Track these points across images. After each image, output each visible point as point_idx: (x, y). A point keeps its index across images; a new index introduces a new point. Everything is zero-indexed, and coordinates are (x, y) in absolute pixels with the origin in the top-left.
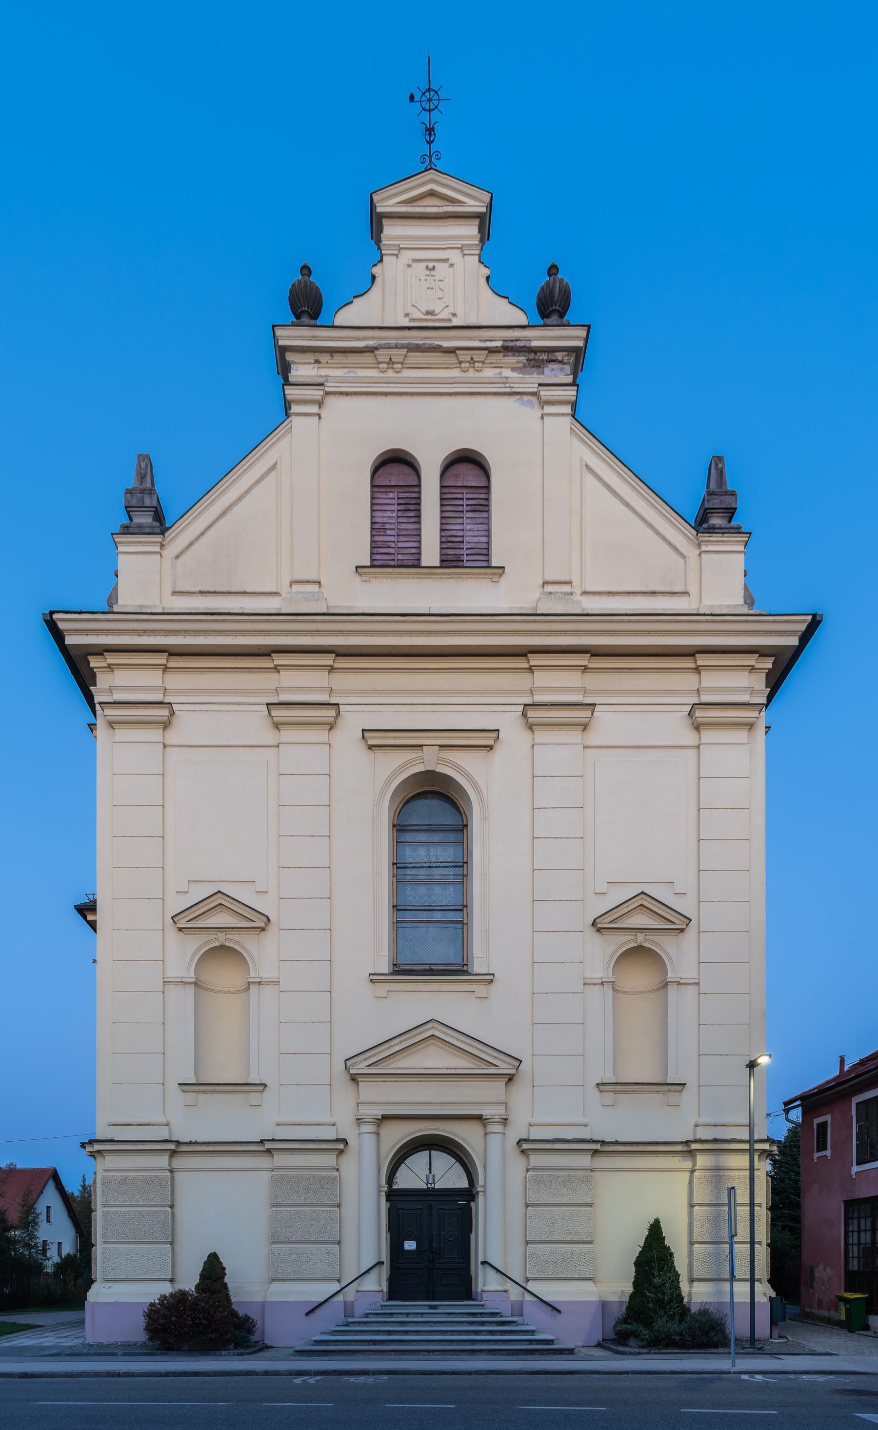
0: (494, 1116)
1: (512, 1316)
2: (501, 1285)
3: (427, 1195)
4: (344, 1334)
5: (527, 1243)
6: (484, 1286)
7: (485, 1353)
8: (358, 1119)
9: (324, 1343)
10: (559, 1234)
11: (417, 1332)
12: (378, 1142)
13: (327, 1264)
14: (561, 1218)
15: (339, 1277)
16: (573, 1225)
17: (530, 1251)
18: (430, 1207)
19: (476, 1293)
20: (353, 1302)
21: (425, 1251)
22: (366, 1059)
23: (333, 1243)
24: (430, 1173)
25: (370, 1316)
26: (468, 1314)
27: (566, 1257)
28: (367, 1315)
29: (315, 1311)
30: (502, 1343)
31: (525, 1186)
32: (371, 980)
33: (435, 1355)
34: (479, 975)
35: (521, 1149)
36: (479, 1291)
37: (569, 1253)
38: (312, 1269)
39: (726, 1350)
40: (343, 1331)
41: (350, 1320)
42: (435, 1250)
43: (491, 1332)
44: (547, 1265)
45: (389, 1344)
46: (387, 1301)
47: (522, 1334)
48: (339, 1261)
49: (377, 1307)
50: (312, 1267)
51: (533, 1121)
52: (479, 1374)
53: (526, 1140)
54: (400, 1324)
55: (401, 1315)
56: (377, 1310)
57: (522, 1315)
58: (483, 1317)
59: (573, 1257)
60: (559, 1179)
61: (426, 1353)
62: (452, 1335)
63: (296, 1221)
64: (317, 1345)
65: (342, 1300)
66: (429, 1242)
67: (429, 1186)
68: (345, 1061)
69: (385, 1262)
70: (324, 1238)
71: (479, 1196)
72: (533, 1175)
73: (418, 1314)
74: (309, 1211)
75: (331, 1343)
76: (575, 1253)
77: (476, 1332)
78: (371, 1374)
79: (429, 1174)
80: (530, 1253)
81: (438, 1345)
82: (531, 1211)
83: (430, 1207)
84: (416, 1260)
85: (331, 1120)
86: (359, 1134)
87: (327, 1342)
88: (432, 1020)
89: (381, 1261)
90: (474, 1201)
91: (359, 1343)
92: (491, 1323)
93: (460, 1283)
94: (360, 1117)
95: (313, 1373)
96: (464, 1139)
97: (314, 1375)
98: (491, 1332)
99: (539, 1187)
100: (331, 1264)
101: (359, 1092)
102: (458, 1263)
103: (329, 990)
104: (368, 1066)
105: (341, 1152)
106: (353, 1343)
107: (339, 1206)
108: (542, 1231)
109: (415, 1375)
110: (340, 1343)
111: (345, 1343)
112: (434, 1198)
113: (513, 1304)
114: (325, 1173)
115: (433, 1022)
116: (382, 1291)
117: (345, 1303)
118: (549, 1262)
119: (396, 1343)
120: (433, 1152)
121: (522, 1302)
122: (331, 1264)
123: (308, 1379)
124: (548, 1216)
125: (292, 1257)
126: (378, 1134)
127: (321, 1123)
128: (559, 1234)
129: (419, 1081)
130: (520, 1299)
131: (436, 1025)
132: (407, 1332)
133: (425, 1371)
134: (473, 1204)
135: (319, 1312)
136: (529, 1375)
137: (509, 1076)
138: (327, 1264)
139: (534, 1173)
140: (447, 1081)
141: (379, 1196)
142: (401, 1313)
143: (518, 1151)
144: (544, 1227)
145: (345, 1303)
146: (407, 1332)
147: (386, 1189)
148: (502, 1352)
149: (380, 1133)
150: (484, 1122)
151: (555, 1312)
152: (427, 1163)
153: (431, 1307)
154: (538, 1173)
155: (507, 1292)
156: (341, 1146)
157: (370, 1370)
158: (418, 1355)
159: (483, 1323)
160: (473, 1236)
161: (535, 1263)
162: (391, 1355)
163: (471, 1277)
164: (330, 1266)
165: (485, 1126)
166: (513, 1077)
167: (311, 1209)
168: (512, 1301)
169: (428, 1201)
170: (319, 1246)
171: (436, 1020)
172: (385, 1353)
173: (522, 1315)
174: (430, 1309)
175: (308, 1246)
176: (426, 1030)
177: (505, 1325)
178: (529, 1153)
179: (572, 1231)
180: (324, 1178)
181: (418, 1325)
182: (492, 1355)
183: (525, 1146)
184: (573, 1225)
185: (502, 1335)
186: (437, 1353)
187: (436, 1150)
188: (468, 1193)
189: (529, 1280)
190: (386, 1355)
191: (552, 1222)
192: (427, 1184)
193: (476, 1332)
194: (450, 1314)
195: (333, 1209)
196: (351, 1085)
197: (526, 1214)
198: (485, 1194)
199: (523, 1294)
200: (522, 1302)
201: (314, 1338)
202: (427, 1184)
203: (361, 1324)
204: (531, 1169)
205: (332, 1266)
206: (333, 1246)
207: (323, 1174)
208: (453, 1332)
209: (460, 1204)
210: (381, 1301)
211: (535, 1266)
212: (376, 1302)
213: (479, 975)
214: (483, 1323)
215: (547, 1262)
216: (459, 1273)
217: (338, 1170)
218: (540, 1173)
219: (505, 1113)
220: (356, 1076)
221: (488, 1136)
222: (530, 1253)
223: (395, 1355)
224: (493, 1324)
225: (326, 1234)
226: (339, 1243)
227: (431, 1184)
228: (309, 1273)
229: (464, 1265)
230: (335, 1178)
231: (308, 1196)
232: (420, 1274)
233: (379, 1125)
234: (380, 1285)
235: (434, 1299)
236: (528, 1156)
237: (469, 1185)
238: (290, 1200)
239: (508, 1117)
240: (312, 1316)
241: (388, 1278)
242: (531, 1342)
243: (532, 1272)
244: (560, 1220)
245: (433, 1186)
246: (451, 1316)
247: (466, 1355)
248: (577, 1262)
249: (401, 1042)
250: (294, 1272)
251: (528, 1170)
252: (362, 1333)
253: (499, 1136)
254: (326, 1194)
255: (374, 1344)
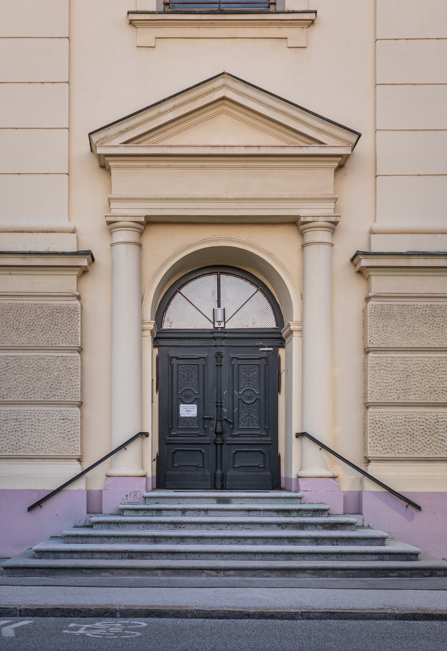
0: (316, 218)
1: (344, 514)
2: (327, 468)
3: (214, 338)
4: (85, 540)
5: (367, 406)
6: (301, 469)
7: (309, 574)
8: (109, 223)
9: (51, 555)
10: (416, 393)
11: (199, 539)
12: (140, 259)
13: (62, 435)
14: (419, 369)
15: (79, 454)
16: (438, 380)
17: (371, 418)
18: (219, 356)
19: (289, 480)
20: (101, 491)
21: (210, 419)
22: (122, 132)
23: (71, 404)
24: (219, 306)
25: (126, 513)
26: (278, 511)
27: (428, 426)
28: (121, 512)
29: (43, 505)
30: (335, 557)
31: (364, 323)
32: (131, 22)
33: (228, 576)
34: (293, 12)
35: (358, 268)
36: (294, 476)
37: (433, 422)
38: (40, 442)
39: (150, 487)
40: (82, 536)
41: (95, 519)
42: (225, 417)
43: (316, 540)
44: (399, 439)
45: (154, 556)
46: (153, 490)
47: (365, 542)
48: (79, 431)
49: (137, 500)
50: (38, 440)
51: (377, 226)
52: (308, 618)
53: (365, 254)
54: (172, 526)
55: (174, 512)
56: (138, 503)
57: (359, 512)
58: (301, 516)
59: (439, 427)
60: (417, 311)
61: (214, 573)
62: (254, 544)
63: (15, 372)
64: (40, 558)
65: (84, 488)
66: (217, 406)
67: (217, 325)
68: (90, 134)
69: (150, 434)
70: (57, 397)
71: (294, 338)
72: (376, 305)
73: (199, 510)
74: (35, 358)
75: (62, 555)
76: (442, 421)
77: (292, 540)
78: (118, 615)
79: (216, 308)
80: (372, 421)
81: (231, 559)
82: (373, 359)
83: (219, 356)
84: (197, 432)
85: (69, 225)
86: (112, 245)
87: (55, 554)
88: (223, 73)
89: (144, 431)
90: (284, 347)
91: (107, 556)
92: (315, 525)
93: (262, 466)
94: (112, 219)
95: (18, 613)
96: (270, 254)
97: (21, 616)
98: (316, 540)
99: (386, 323)
100: (67, 435)
101: (111, 184)
102: (261, 436)
103: (68, 36)
104: (125, 143)
105: (84, 272)
106: (97, 555)
107: (80, 350)
108: (390, 387)
109: (196, 617)
110: (75, 555)
111: (84, 555)
112: (223, 343)
113: (346, 497)
114: (59, 302)
115: (224, 77)
116: (145, 476)
117: (89, 493)
118: (401, 434)
119: (164, 556)
120: (223, 277)
121: (359, 495)
122: (67, 435)
123: (6, 625)
124: (400, 366)
125: (8, 425)
126: (140, 245)
127: (54, 230)
128: (416, 393)
129: (203, 167)
130: (357, 488)
131: (230, 82)
132: (182, 539)
133: (212, 611)
134: (281, 352)
135: (48, 506)
136: (398, 622)
137: (340, 159)
138: (62, 435)
139: (378, 303)
140: (245, 167)
141: (142, 336)
142: (175, 510)
143: (352, 271)
144: (394, 382)
145: (89, 493)
146: (182, 539)
147: (152, 326)
148: (335, 572)
149: (143, 244)
150: (302, 227)
151: (411, 508)
152: (213, 293)
153: (221, 500)
154: (383, 303)
155: (337, 479)
156: (84, 262)
157: (117, 608)
158: (200, 576)
159: (302, 526)
160: (281, 398)
161: (380, 436)
162: (157, 575)
163: (279, 458)
164: (66, 439)
165: (302, 234)
166: (345, 162)
167: (38, 354)
168: (344, 492)
169: (215, 346)
170: (49, 409)
171: (229, 74)
172: (148, 572)
173: (359, 512)
174: (218, 503)
175: (33, 408)
176: (214, 89)
177: (337, 529)
178: (371, 273)
179: (437, 389)
180: (59, 310)
181: (199, 526)
182: (319, 577)
183: (365, 262)
184: (438, 380)
185: (333, 545)
186: (231, 573)
187: (227, 274)
188: (276, 336)
189: (369, 461)
190: (148, 575)
191: (405, 376)
192: (214, 323)
193: (292, 540)
194: (249, 510)
195: (70, 355)
196: (100, 174)
197: (365, 364)
198: (302, 334)
199: (361, 482)
200: (359, 495)
201: (36, 547)
202: (214, 323)
203: (112, 526)
204: (374, 297)
205: (69, 439)
206: (71, 409)
207: (56, 303)
208: (255, 540)
209: (262, 351)
210: (144, 490)
211: (380, 440)
212: (135, 493)
213: (293, 12)
214: (302, 526)
215: (399, 435)
216: (261, 451)
217: (79, 298)
218: (387, 303)
219: (334, 213)
220: (107, 159)
221: (308, 249)
222: (372, 421)
223: (163, 575)
224: (319, 527)
225: (61, 391)
226: (80, 405)
227: (219, 322)
228: (35, 449)
229: (269, 439)
230: (75, 309)
231: (33, 335)
232: (203, 451)
233: (141, 233)
234: (142, 467)
235: (223, 488)
236: (368, 279)
237: (277, 325)
238: (6, 342)
239: (338, 219)
240: (38, 512)
241: (155, 457)
242: (381, 555)
243: (375, 448)
244: (418, 373)
245: (222, 325)
246: (252, 513)
247: (278, 576)
248: (444, 435)
249: (175, 107)
250: (11, 447)
251: (368, 299)
252: (112, 539)
253: (324, 249)
254: (61, 333)
255: (130, 558)
